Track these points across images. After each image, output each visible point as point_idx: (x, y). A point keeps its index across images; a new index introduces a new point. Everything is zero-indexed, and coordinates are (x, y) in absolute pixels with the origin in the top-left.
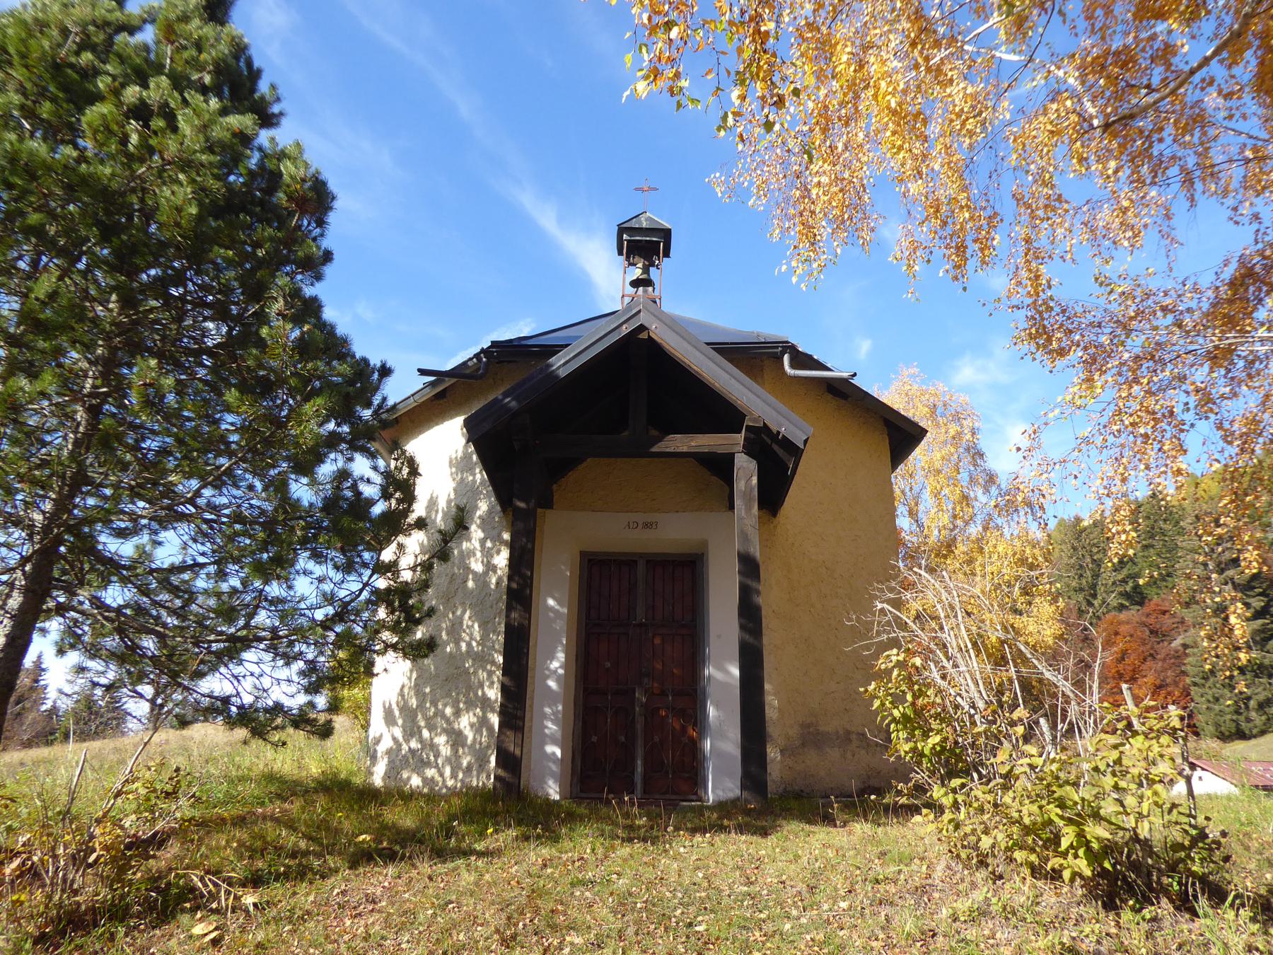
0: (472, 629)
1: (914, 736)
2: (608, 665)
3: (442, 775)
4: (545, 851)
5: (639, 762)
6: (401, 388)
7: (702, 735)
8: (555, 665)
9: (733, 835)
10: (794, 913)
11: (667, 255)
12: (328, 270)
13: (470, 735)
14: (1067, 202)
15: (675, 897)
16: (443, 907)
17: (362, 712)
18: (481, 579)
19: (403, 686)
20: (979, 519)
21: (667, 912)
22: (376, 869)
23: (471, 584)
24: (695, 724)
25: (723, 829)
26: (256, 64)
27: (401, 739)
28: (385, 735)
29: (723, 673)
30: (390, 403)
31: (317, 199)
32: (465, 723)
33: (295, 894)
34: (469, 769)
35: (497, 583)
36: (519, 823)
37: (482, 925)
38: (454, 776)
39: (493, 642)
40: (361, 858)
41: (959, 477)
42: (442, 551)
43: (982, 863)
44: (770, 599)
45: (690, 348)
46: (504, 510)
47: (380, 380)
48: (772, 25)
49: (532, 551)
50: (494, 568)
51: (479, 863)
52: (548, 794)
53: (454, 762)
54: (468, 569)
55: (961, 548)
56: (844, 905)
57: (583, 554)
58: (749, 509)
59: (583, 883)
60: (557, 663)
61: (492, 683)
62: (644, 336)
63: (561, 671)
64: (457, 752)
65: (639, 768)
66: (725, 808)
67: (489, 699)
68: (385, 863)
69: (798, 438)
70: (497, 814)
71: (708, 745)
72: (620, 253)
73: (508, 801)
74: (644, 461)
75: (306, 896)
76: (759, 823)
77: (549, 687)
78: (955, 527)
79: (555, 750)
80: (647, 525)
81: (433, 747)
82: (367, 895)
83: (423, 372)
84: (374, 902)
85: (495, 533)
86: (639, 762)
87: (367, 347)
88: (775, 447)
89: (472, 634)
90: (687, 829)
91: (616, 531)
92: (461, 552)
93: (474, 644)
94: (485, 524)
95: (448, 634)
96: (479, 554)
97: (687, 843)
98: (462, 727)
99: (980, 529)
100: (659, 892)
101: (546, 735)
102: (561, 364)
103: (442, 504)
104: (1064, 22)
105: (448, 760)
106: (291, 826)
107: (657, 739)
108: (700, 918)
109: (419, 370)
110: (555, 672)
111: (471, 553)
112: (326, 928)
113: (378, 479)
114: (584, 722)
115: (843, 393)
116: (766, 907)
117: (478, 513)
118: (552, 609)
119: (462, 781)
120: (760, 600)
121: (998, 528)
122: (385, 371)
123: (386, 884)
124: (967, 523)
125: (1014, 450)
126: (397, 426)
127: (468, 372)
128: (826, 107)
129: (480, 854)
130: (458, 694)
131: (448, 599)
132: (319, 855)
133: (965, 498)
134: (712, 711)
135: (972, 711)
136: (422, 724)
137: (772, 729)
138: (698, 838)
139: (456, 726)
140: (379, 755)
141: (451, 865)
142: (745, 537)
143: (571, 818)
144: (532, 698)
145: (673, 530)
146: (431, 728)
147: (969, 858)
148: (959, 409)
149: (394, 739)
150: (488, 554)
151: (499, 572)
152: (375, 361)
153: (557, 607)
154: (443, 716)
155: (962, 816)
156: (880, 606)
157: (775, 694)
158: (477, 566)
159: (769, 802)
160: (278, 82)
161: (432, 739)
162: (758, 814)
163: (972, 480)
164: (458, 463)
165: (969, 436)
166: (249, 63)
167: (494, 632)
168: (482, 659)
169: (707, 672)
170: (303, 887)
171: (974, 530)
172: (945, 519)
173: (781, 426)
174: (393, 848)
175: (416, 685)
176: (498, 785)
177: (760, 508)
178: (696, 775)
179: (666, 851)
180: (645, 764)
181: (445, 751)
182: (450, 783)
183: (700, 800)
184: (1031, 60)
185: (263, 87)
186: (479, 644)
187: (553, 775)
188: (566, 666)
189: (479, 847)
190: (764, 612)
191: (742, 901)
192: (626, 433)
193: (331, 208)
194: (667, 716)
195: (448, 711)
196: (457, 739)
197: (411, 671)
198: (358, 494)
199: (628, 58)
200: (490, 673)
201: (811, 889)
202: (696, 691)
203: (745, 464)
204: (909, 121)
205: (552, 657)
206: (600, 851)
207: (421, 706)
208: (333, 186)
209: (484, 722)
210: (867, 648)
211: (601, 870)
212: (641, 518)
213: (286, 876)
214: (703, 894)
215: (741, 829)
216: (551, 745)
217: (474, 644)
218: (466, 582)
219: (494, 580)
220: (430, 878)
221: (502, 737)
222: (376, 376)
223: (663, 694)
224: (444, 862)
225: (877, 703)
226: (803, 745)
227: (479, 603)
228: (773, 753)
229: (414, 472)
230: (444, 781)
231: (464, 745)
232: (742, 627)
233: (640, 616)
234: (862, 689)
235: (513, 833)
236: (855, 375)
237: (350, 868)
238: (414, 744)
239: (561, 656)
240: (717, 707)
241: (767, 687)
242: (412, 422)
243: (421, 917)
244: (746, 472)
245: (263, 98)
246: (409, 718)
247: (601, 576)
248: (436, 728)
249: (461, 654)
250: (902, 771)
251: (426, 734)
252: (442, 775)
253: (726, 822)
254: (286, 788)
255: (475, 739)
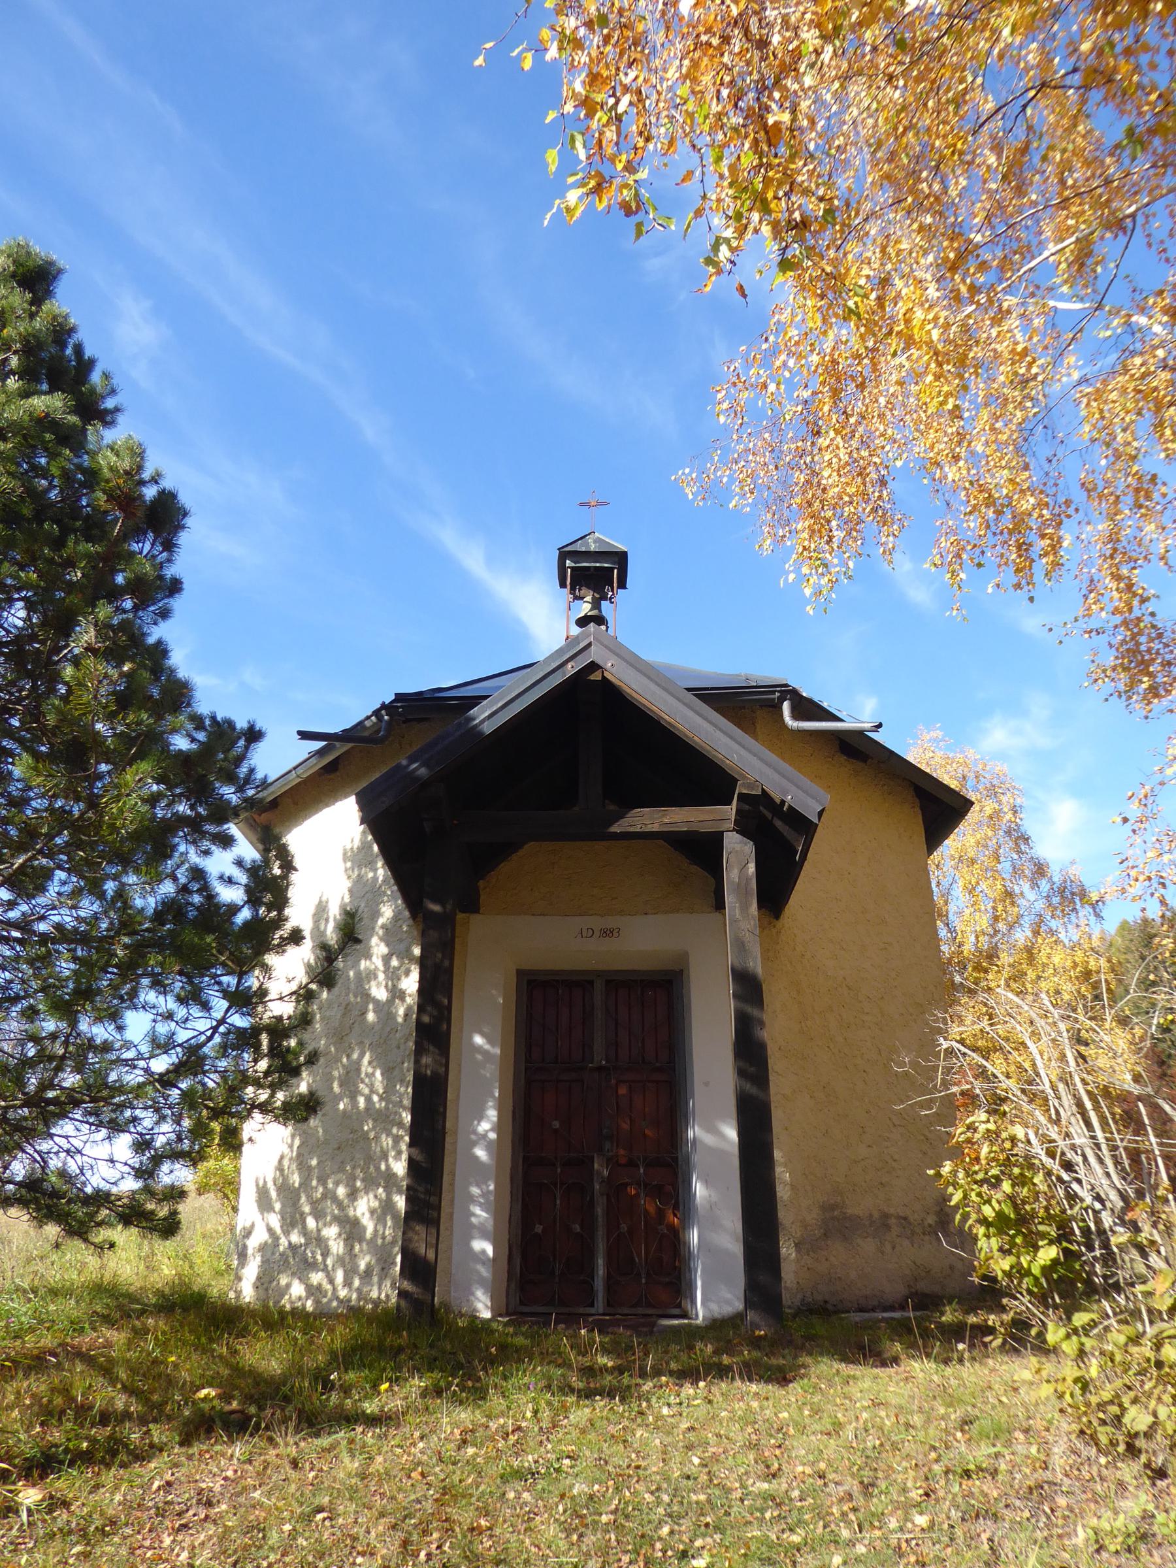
0: (373, 1078)
1: (1013, 1244)
2: (556, 1124)
3: (331, 1281)
4: (465, 1416)
5: (600, 1262)
6: (277, 758)
7: (686, 1224)
8: (484, 1126)
9: (738, 1383)
10: (845, 1534)
11: (622, 585)
12: (177, 603)
13: (369, 1225)
14: (1164, 484)
15: (659, 1502)
16: (307, 1518)
17: (228, 1188)
18: (385, 1010)
19: (282, 1157)
20: (1026, 922)
21: (647, 1530)
22: (218, 1448)
23: (371, 1016)
24: (676, 1207)
25: (722, 1372)
26: (88, 353)
27: (278, 1231)
28: (257, 1222)
29: (714, 1134)
30: (259, 775)
31: (164, 517)
32: (363, 1208)
33: (97, 1487)
34: (368, 1273)
35: (406, 1015)
36: (431, 1365)
37: (363, 1554)
38: (348, 1283)
39: (401, 1096)
40: (201, 1427)
41: (999, 867)
42: (325, 972)
43: (1132, 1451)
44: (776, 1031)
45: (658, 691)
46: (414, 916)
47: (247, 748)
48: (786, 117)
49: (450, 972)
50: (401, 995)
51: (369, 1438)
52: (475, 1310)
53: (348, 1262)
54: (367, 996)
55: (1005, 958)
56: (922, 1520)
57: (520, 973)
58: (745, 908)
59: (519, 1474)
60: (485, 1126)
61: (399, 1153)
62: (596, 676)
63: (493, 1136)
64: (352, 1248)
65: (601, 1271)
66: (717, 1327)
67: (395, 1175)
68: (230, 1437)
69: (809, 808)
70: (400, 1350)
71: (694, 1236)
72: (563, 585)
73: (418, 1335)
74: (599, 846)
75: (112, 1492)
76: (774, 1361)
77: (477, 1158)
78: (996, 932)
79: (484, 1246)
80: (607, 933)
81: (320, 1241)
82: (200, 1492)
83: (305, 735)
84: (209, 1504)
85: (402, 946)
86: (600, 1262)
87: (216, 694)
88: (778, 823)
89: (375, 1085)
90: (671, 1373)
91: (564, 941)
92: (358, 974)
93: (375, 1098)
94: (390, 935)
95: (341, 1086)
96: (381, 976)
97: (672, 1400)
98: (359, 1213)
99: (1029, 934)
100: (635, 1493)
101: (472, 1226)
102: (486, 718)
103: (334, 911)
104: (1149, 245)
105: (340, 1261)
106: (107, 1371)
107: (624, 1227)
108: (698, 1543)
109: (299, 733)
110: (484, 1136)
111: (372, 975)
112: (132, 1551)
113: (243, 878)
114: (525, 1206)
115: (859, 752)
116: (800, 1522)
117: (381, 921)
118: (479, 1049)
119: (359, 1290)
120: (765, 1035)
121: (1052, 932)
122: (254, 735)
123: (230, 1473)
124: (1011, 927)
125: (1119, 820)
126: (274, 812)
127: (366, 734)
128: (835, 362)
129: (372, 1421)
130: (354, 1168)
131: (340, 1037)
132: (143, 1421)
133: (1009, 894)
134: (699, 1189)
135: (1098, 1206)
136: (307, 1209)
137: (785, 1216)
138: (688, 1390)
139: (351, 1213)
140: (250, 1252)
141: (325, 1441)
142: (740, 946)
143: (507, 1356)
144: (453, 1174)
145: (642, 938)
146: (318, 1215)
147: (1113, 1444)
148: (995, 782)
149: (270, 1230)
150: (394, 976)
151: (409, 1000)
152: (241, 724)
153: (487, 1047)
154: (335, 1198)
155: (1094, 1372)
156: (945, 1045)
157: (785, 1166)
158: (380, 993)
159: (787, 1328)
160: (110, 368)
161: (319, 1231)
162: (772, 1345)
163: (1016, 871)
164: (354, 855)
165: (1009, 816)
166: (79, 349)
167: (402, 1081)
168: (385, 1119)
169: (690, 1134)
170: (109, 1476)
171: (1022, 936)
172: (984, 922)
173: (786, 793)
174: (252, 1410)
175: (299, 1155)
176: (403, 1303)
177: (760, 907)
178: (679, 1278)
179: (641, 1413)
180: (608, 1265)
181: (337, 1247)
182: (343, 1293)
183: (685, 1316)
184: (1099, 307)
185: (96, 377)
186: (381, 1099)
187: (482, 1282)
188: (498, 1128)
189: (370, 1407)
190: (769, 1052)
191: (762, 1511)
192: (576, 809)
193: (183, 527)
194: (637, 1195)
195: (341, 1191)
196: (352, 1230)
197: (293, 1136)
198: (210, 897)
199: (552, 157)
200: (397, 1140)
201: (867, 1488)
202: (676, 1160)
203: (738, 847)
204: (956, 358)
205: (481, 1117)
206: (546, 1414)
207: (305, 1183)
208: (185, 499)
209: (387, 1206)
210: (928, 1104)
211: (551, 1446)
212: (596, 923)
213: (84, 1458)
214: (702, 1497)
215: (751, 1372)
216: (479, 1237)
217: (375, 1098)
218: (364, 1013)
219: (401, 1011)
220: (295, 1464)
221: (410, 1234)
222: (242, 743)
223: (632, 1164)
224: (317, 1435)
225: (957, 1197)
226: (825, 1235)
227: (381, 1042)
228: (787, 1250)
229: (288, 866)
230: (334, 1289)
231: (361, 1240)
232: (741, 1073)
233: (600, 1058)
234: (931, 1172)
235: (417, 1383)
236: (880, 725)
237: (181, 1444)
238: (296, 1238)
239: (492, 1114)
240: (706, 1183)
241: (777, 1155)
242: (296, 803)
243: (274, 1538)
244: (740, 858)
245: (93, 391)
246: (288, 1199)
247: (547, 1005)
248: (325, 1215)
249: (359, 1112)
250: (991, 1294)
251: (311, 1223)
252: (331, 1281)
253: (726, 1360)
254: (119, 1305)
255: (376, 1231)
